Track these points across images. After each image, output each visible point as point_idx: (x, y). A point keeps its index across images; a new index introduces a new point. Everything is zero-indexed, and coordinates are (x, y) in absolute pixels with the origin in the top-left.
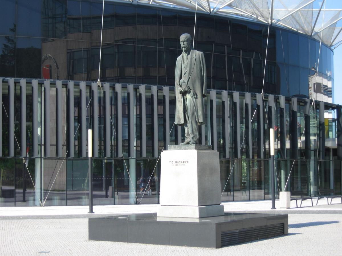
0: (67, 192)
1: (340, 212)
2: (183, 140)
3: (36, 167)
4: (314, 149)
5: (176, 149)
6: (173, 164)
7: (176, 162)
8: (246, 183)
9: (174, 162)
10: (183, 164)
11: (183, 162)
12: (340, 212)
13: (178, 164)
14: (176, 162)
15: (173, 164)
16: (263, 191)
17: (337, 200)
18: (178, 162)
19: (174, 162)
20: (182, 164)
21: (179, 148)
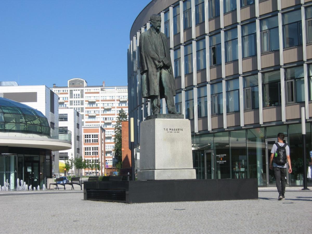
0: (96, 158)
1: (200, 5)
2: (41, 126)
3: (257, 153)
4: (269, 82)
5: (166, 117)
6: (168, 131)
7: (170, 129)
8: (211, 179)
9: (169, 129)
10: (177, 131)
11: (177, 129)
12: (200, 5)
13: (173, 131)
14: (170, 129)
15: (168, 131)
16: (230, 146)
17: (220, 1)
18: (173, 130)
19: (169, 129)
20: (177, 131)
21: (168, 117)
